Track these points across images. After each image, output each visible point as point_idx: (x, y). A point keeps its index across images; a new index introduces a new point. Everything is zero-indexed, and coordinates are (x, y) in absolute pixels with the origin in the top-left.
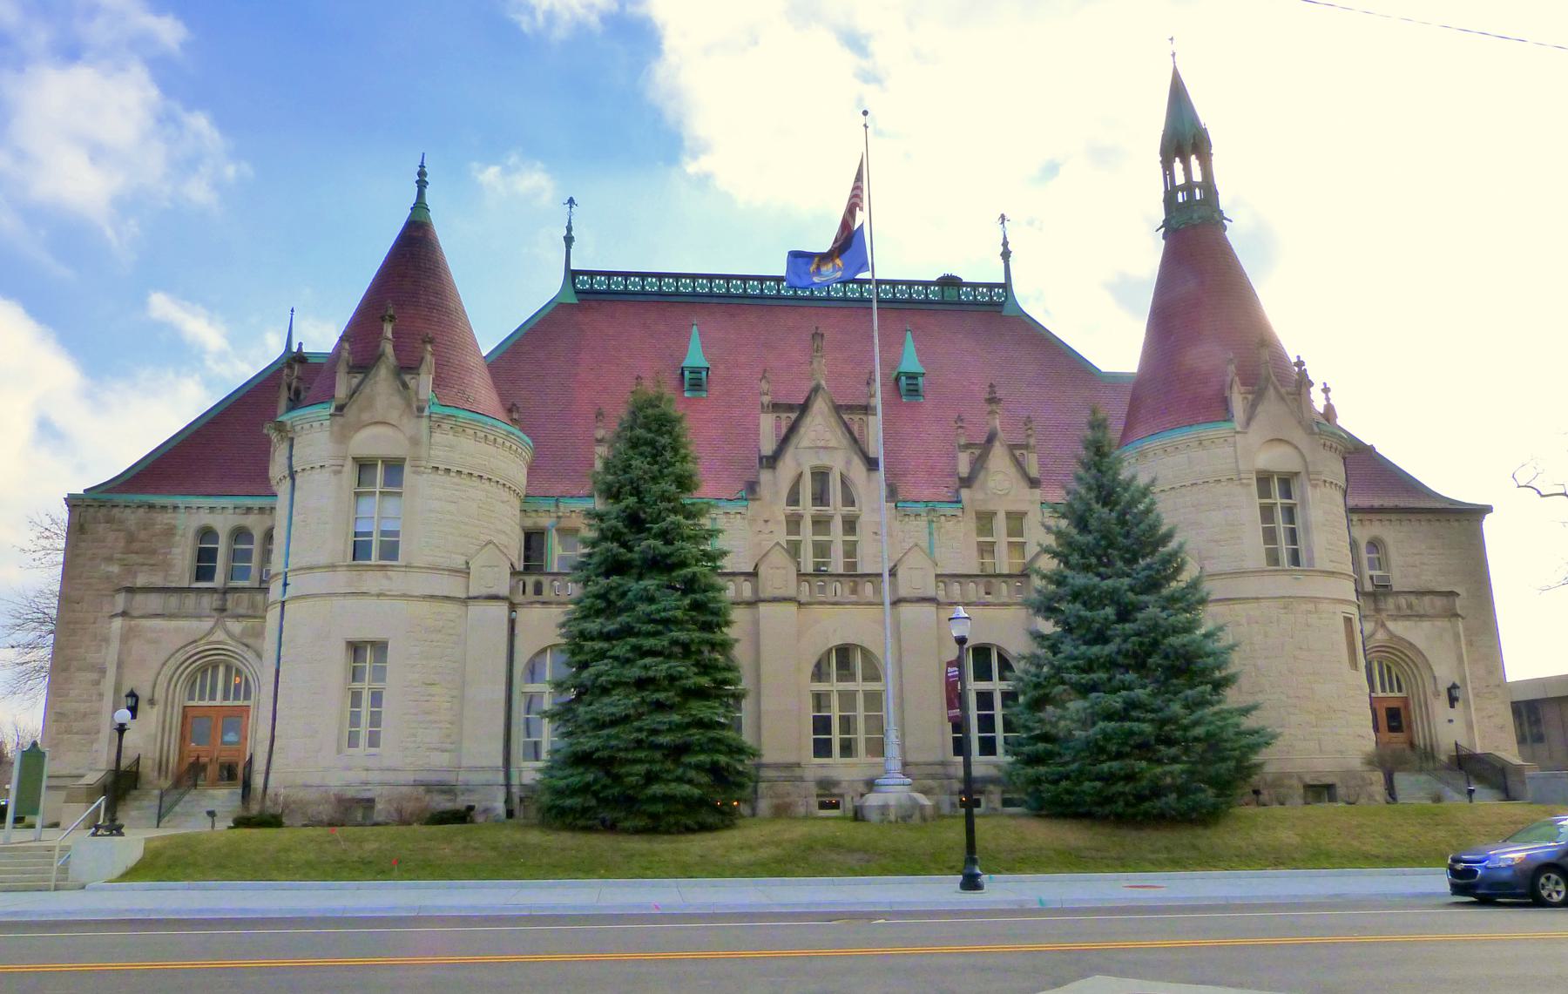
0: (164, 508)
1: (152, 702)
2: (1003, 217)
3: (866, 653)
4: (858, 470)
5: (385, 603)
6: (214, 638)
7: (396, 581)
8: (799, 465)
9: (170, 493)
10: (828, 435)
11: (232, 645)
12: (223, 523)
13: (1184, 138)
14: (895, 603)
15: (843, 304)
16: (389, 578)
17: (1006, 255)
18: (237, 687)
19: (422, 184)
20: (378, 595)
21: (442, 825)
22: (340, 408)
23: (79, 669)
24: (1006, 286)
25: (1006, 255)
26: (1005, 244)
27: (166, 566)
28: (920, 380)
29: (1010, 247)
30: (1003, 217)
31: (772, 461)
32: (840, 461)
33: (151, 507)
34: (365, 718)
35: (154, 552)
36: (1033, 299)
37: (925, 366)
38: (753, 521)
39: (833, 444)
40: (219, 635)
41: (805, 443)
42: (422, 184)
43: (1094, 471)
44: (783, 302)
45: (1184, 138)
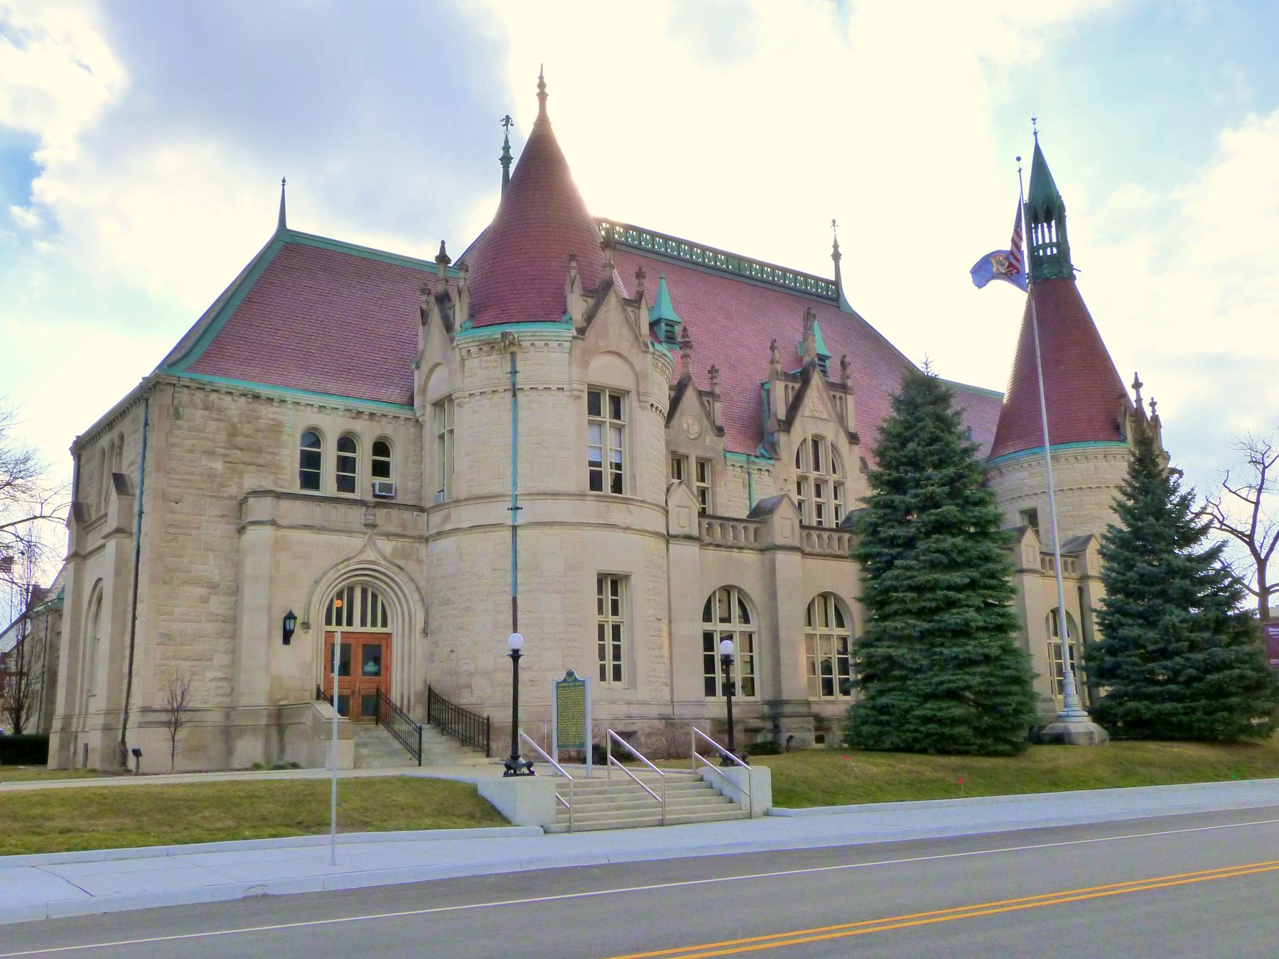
1: (306, 625)
2: (834, 221)
3: (740, 591)
4: (843, 443)
5: (628, 536)
6: (364, 557)
7: (618, 513)
8: (805, 432)
9: (274, 384)
10: (821, 408)
11: (383, 567)
12: (333, 427)
14: (514, 528)
15: (700, 269)
16: (630, 512)
17: (836, 256)
18: (339, 611)
19: (542, 96)
20: (625, 529)
22: (582, 331)
23: (184, 583)
24: (837, 283)
25: (836, 256)
26: (836, 246)
27: (274, 468)
28: (827, 362)
30: (834, 221)
31: (787, 425)
32: (830, 432)
33: (257, 397)
34: (609, 652)
35: (259, 451)
36: (857, 298)
37: (829, 349)
38: (776, 479)
39: (825, 416)
40: (370, 555)
41: (807, 413)
44: (641, 253)
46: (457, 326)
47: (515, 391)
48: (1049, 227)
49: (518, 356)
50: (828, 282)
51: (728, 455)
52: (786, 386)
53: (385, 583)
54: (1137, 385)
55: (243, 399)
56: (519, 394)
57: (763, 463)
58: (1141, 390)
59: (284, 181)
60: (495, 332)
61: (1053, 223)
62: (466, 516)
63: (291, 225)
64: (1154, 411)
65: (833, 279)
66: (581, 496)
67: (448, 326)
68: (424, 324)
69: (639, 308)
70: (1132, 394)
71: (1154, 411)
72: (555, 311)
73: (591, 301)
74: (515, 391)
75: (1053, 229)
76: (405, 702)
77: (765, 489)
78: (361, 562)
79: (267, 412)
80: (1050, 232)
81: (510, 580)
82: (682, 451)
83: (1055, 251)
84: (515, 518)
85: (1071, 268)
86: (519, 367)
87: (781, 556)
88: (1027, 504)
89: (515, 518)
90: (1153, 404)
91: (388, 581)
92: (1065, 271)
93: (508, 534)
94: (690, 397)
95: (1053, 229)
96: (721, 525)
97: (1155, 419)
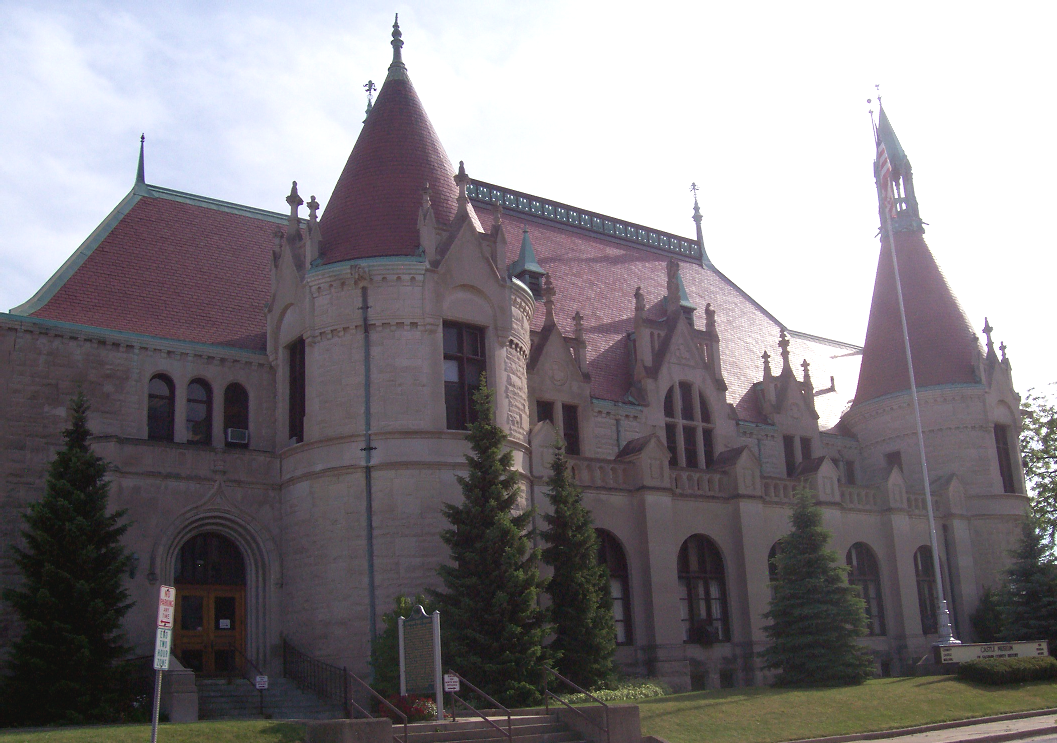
0: (116, 345)
2: (694, 185)
13: (893, 167)
14: (368, 470)
15: (579, 231)
17: (697, 218)
19: (397, 43)
21: (444, 689)
22: (435, 264)
24: (699, 242)
25: (697, 218)
26: (696, 208)
29: (701, 212)
30: (694, 185)
33: (102, 343)
42: (397, 43)
43: (555, 432)
45: (893, 167)
46: (308, 266)
47: (367, 327)
48: (898, 185)
49: (370, 292)
50: (690, 241)
51: (594, 401)
52: (652, 334)
53: (229, 527)
54: (988, 330)
55: (88, 344)
56: (360, 322)
57: (632, 411)
58: (992, 334)
59: (143, 138)
60: (344, 269)
61: (901, 181)
62: (320, 460)
63: (148, 181)
64: (1004, 354)
65: (694, 237)
66: (436, 434)
67: (299, 265)
68: (276, 266)
69: (495, 242)
70: (983, 340)
71: (1004, 354)
72: (409, 246)
73: (445, 235)
74: (367, 327)
75: (902, 187)
76: (261, 656)
77: (632, 432)
78: (210, 510)
79: (115, 358)
80: (898, 189)
81: (364, 524)
82: (548, 397)
83: (904, 206)
84: (368, 459)
85: (920, 222)
86: (370, 303)
87: (651, 498)
88: (892, 448)
89: (368, 459)
90: (1003, 348)
91: (228, 523)
92: (914, 224)
93: (360, 476)
94: (553, 347)
95: (902, 187)
96: (588, 466)
97: (1006, 361)
